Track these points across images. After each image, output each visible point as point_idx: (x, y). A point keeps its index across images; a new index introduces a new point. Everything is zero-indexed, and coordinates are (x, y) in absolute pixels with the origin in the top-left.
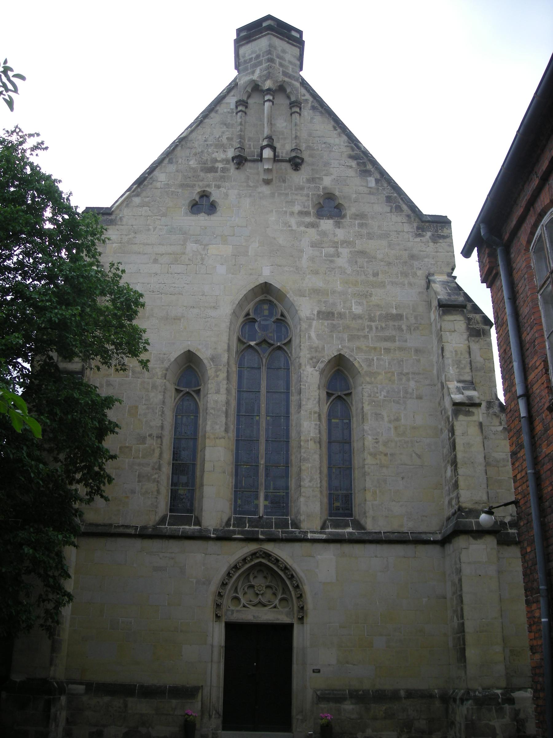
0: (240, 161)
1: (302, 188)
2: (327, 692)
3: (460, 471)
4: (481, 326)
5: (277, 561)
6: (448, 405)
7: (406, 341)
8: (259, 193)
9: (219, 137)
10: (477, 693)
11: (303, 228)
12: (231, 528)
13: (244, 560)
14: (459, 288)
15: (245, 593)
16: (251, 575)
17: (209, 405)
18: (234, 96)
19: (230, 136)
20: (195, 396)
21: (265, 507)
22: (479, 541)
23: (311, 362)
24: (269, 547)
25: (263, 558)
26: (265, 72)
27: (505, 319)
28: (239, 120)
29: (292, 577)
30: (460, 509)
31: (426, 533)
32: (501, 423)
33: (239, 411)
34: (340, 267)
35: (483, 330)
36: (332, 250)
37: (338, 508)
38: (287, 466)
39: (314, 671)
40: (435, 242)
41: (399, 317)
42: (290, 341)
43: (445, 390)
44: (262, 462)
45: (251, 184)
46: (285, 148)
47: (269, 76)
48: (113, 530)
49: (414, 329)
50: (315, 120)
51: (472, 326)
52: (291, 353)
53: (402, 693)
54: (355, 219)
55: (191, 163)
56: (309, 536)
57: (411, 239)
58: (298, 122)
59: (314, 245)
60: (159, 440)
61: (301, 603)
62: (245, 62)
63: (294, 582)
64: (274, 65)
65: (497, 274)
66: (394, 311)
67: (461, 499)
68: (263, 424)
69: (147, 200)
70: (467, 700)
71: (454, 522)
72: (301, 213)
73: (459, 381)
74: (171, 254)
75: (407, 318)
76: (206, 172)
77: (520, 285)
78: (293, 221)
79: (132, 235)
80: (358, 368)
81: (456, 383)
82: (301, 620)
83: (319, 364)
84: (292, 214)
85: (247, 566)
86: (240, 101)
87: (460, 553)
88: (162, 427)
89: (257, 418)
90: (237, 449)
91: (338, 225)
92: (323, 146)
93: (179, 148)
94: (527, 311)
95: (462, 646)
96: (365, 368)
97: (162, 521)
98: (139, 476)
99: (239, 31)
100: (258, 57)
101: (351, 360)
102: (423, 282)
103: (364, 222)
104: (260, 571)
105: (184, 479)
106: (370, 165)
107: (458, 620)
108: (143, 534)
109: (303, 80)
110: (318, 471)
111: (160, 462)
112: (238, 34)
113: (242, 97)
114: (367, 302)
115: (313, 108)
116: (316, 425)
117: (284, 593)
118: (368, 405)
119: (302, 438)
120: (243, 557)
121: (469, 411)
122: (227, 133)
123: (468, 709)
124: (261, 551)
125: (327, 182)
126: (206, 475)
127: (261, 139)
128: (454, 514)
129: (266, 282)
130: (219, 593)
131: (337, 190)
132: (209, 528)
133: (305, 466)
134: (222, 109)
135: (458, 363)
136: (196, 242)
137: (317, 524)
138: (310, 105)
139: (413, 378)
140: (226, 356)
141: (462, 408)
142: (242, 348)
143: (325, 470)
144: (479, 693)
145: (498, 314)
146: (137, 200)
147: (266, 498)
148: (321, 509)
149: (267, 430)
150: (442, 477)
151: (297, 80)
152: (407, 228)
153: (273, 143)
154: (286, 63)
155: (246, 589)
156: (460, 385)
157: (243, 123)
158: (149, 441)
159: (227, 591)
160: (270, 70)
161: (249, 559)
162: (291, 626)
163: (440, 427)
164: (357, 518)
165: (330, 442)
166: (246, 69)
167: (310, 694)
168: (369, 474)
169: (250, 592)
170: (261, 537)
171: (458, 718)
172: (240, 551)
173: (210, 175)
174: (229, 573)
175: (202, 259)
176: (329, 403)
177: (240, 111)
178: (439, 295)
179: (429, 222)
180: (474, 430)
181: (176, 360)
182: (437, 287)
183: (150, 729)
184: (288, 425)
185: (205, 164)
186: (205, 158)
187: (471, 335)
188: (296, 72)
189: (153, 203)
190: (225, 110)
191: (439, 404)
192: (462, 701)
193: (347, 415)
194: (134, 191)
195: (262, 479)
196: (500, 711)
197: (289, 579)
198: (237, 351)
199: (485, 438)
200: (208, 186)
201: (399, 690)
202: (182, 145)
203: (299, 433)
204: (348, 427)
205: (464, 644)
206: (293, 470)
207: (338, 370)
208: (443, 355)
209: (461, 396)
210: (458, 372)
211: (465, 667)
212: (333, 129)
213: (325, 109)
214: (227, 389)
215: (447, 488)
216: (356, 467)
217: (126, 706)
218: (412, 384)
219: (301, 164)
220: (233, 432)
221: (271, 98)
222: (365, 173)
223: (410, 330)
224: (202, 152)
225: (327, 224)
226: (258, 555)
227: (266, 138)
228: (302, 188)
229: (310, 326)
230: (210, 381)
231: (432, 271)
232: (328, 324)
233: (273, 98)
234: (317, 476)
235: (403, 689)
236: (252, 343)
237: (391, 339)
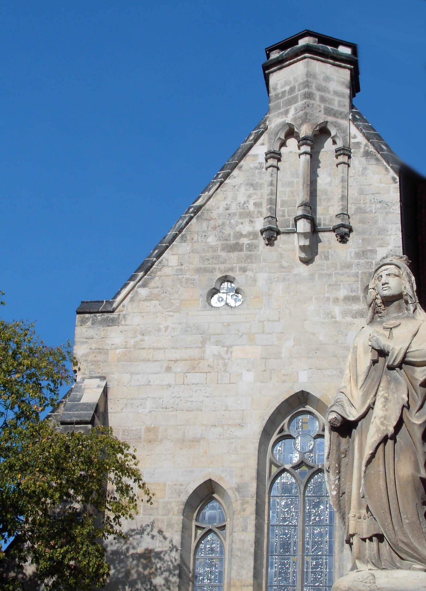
11: (349, 319)
47: (305, 119)
78: (337, 310)
84: (336, 300)
100: (292, 90)
138: (362, 150)
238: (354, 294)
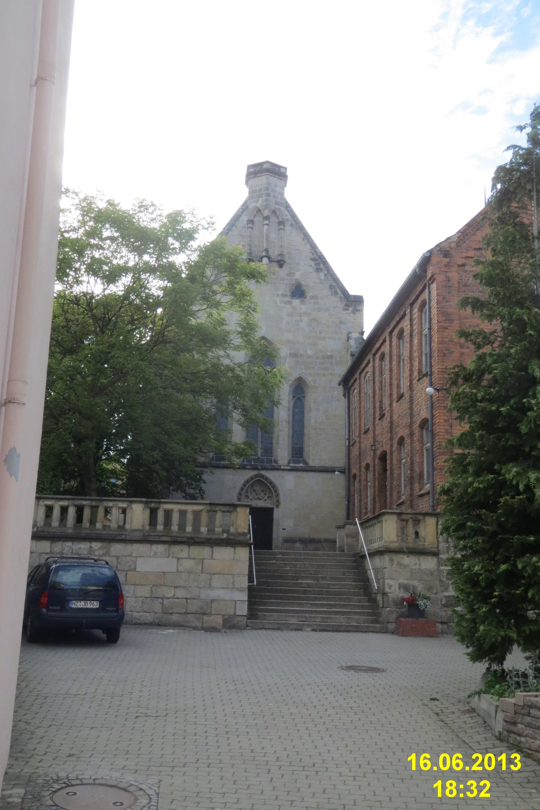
5: (267, 479)
7: (334, 370)
11: (283, 305)
13: (252, 478)
21: (261, 453)
24: (263, 472)
28: (249, 234)
29: (273, 486)
36: (298, 318)
41: (331, 357)
47: (266, 207)
53: (322, 540)
54: (312, 299)
56: (282, 467)
59: (290, 315)
64: (269, 198)
66: (329, 354)
78: (278, 300)
82: (277, 506)
84: (278, 295)
91: (302, 303)
99: (249, 167)
100: (260, 190)
102: (345, 337)
115: (292, 225)
125: (298, 275)
134: (239, 224)
138: (290, 223)
143: (291, 436)
153: (268, 254)
162: (273, 509)
167: (281, 540)
170: (259, 467)
172: (249, 474)
177: (250, 227)
193: (302, 407)
204: (303, 413)
222: (318, 270)
225: (296, 302)
231: (351, 331)
234: (286, 439)
238: (285, 293)
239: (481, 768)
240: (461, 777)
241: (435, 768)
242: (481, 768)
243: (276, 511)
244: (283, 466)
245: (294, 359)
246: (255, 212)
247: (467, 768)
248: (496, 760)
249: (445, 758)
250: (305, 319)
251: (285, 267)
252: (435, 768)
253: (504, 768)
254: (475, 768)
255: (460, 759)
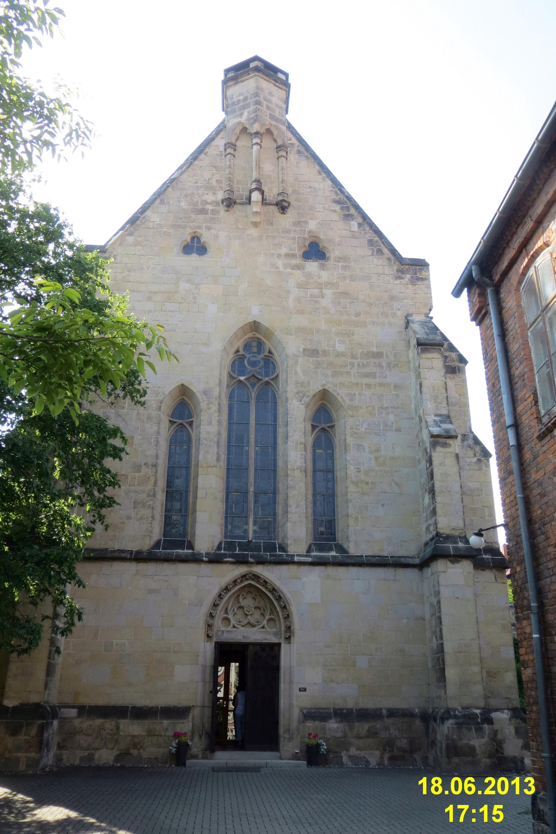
0: (230, 203)
1: (289, 231)
2: (313, 711)
3: (438, 499)
4: (457, 364)
6: (425, 436)
7: (386, 377)
8: (249, 235)
9: (209, 180)
10: (457, 712)
11: (289, 270)
12: (222, 551)
13: (235, 582)
14: (436, 328)
15: (235, 614)
16: (241, 596)
17: (201, 436)
18: (222, 138)
19: (219, 178)
20: (188, 427)
21: (255, 532)
22: (457, 565)
23: (297, 396)
25: (252, 580)
26: (253, 115)
27: (494, 355)
28: (228, 163)
29: (279, 598)
30: (438, 535)
31: (405, 557)
32: (475, 455)
33: (229, 441)
34: (324, 308)
35: (459, 367)
36: (316, 291)
37: (322, 533)
38: (275, 492)
39: (300, 690)
40: (413, 284)
41: (379, 355)
42: (277, 376)
43: (423, 423)
44: (252, 489)
45: (240, 226)
46: (272, 193)
47: (256, 119)
48: (109, 555)
49: (394, 366)
50: (301, 165)
51: (448, 364)
52: (278, 388)
53: (384, 712)
55: (182, 204)
56: (296, 559)
57: (391, 281)
58: (284, 165)
59: (300, 286)
60: (155, 468)
61: (288, 623)
62: (233, 103)
63: (282, 603)
64: (261, 108)
65: (487, 313)
66: (375, 350)
67: (439, 526)
68: (252, 455)
69: (140, 239)
70: (448, 719)
71: (433, 547)
72: (287, 255)
73: (436, 415)
74: (164, 292)
75: (387, 356)
76: (197, 214)
77: (510, 323)
78: (280, 263)
79: (127, 273)
80: (341, 402)
81: (433, 416)
82: (288, 639)
83: (305, 399)
84: (279, 256)
85: (237, 588)
86: (229, 143)
87: (438, 576)
88: (157, 457)
89: (247, 448)
90: (228, 477)
92: (309, 190)
93: (170, 189)
94: (516, 348)
95: (442, 666)
96: (348, 402)
97: (157, 545)
98: (134, 503)
99: (227, 71)
100: (245, 99)
101: (335, 394)
102: (402, 322)
103: (347, 264)
104: (249, 592)
105: (177, 505)
106: (353, 209)
107: (437, 641)
108: (139, 557)
109: (289, 123)
110: (304, 498)
111: (154, 489)
112: (226, 75)
113: (230, 140)
114: (349, 340)
115: (299, 152)
116: (302, 455)
117: (272, 613)
118: (351, 436)
119: (289, 467)
120: (234, 580)
121: (446, 443)
122: (217, 175)
123: (448, 728)
124: (250, 573)
125: (312, 225)
126: (199, 502)
127: (249, 182)
128: (432, 540)
129: (255, 321)
130: (211, 614)
131: (322, 234)
132: (202, 552)
133: (292, 493)
134: (211, 150)
135: (435, 398)
136: (189, 281)
137: (303, 549)
138: (296, 149)
139: (392, 412)
140: (218, 389)
141: (439, 440)
142: (233, 383)
143: (310, 497)
144: (459, 712)
145: (486, 351)
146: (130, 239)
147: (255, 523)
148: (307, 533)
149: (256, 460)
150: (419, 505)
151: (283, 124)
152: (387, 270)
154: (273, 106)
155: (236, 609)
156: (438, 419)
157: (232, 166)
158: (144, 470)
159: (218, 612)
160: (258, 113)
161: (239, 581)
162: (279, 645)
163: (418, 458)
164: (340, 542)
165: (314, 471)
166: (234, 111)
167: (296, 713)
168: (351, 501)
169: (240, 612)
170: (250, 560)
171: (439, 737)
172: (231, 572)
173: (201, 217)
174: (220, 594)
175: (195, 298)
176: (314, 435)
177: (229, 154)
178: (417, 334)
179: (408, 265)
180: (450, 461)
181: (170, 393)
182: (415, 326)
183: (141, 751)
184: (275, 455)
185: (196, 205)
186: (196, 200)
187: (447, 372)
188: (283, 116)
189: (146, 243)
190: (215, 153)
191: (417, 436)
192: (443, 719)
194: (127, 230)
195: (251, 505)
196: (479, 730)
197: (277, 599)
198: (228, 386)
199: (460, 468)
200: (200, 227)
201: (381, 709)
202: (173, 186)
203: (286, 463)
205: (444, 664)
206: (280, 498)
207: (322, 403)
208: (421, 390)
209: (438, 429)
210: (436, 406)
211: (445, 685)
212: (317, 173)
213: (310, 154)
214: (218, 421)
215: (425, 514)
216: (339, 495)
217: (118, 728)
218: (391, 417)
219: (287, 208)
220: (224, 461)
221: (259, 141)
222: (348, 217)
223: (390, 366)
224: (193, 193)
225: (312, 266)
226: (247, 577)
227: (255, 181)
228: (289, 231)
229: (296, 362)
230: (202, 413)
232: (313, 361)
233: (261, 142)
234: (303, 503)
235: (385, 708)
236: (242, 378)
237: (372, 375)
239: (493, 793)
240: (476, 801)
241: (447, 792)
242: (493, 793)
243: (284, 648)
244: (298, 555)
245: (311, 359)
246: (238, 131)
247: (480, 792)
248: (510, 783)
249: (456, 782)
250: (329, 292)
251: (290, 212)
252: (447, 792)
253: (518, 792)
254: (488, 792)
255: (473, 783)
